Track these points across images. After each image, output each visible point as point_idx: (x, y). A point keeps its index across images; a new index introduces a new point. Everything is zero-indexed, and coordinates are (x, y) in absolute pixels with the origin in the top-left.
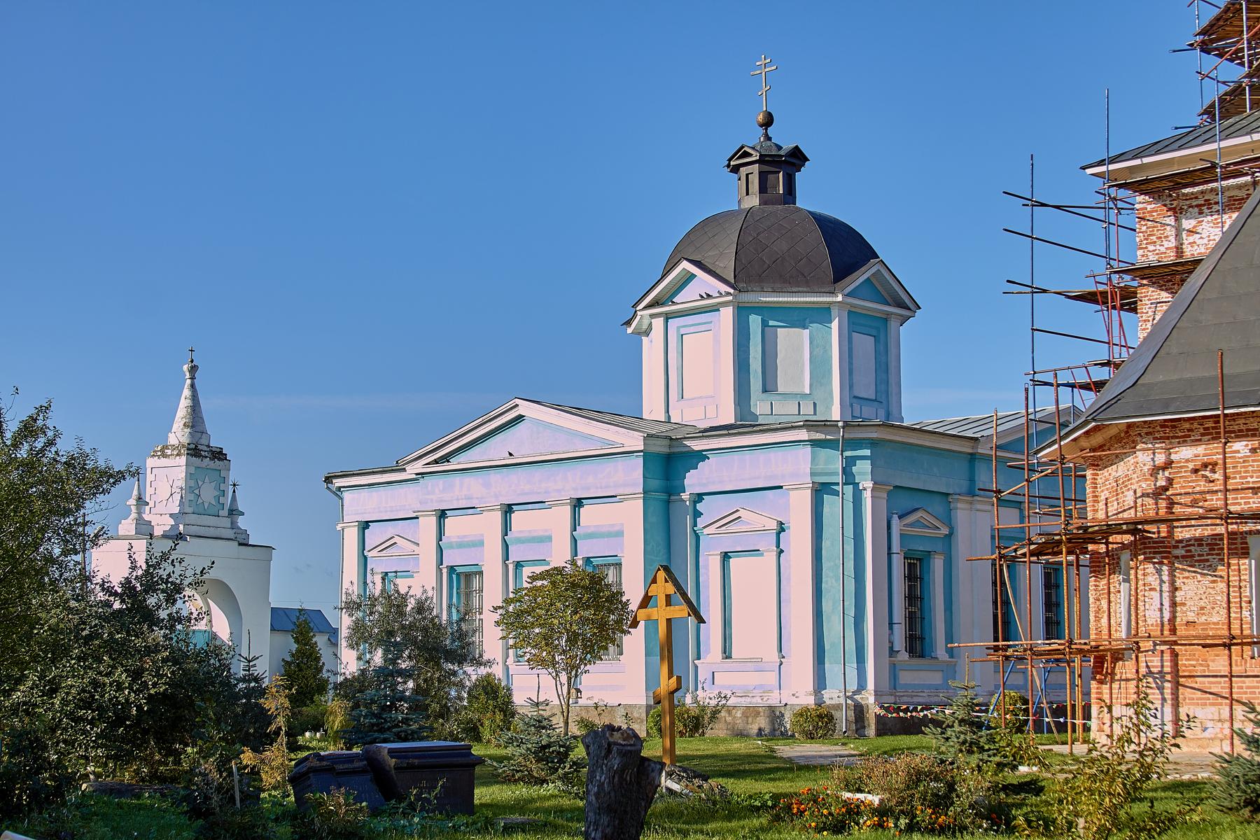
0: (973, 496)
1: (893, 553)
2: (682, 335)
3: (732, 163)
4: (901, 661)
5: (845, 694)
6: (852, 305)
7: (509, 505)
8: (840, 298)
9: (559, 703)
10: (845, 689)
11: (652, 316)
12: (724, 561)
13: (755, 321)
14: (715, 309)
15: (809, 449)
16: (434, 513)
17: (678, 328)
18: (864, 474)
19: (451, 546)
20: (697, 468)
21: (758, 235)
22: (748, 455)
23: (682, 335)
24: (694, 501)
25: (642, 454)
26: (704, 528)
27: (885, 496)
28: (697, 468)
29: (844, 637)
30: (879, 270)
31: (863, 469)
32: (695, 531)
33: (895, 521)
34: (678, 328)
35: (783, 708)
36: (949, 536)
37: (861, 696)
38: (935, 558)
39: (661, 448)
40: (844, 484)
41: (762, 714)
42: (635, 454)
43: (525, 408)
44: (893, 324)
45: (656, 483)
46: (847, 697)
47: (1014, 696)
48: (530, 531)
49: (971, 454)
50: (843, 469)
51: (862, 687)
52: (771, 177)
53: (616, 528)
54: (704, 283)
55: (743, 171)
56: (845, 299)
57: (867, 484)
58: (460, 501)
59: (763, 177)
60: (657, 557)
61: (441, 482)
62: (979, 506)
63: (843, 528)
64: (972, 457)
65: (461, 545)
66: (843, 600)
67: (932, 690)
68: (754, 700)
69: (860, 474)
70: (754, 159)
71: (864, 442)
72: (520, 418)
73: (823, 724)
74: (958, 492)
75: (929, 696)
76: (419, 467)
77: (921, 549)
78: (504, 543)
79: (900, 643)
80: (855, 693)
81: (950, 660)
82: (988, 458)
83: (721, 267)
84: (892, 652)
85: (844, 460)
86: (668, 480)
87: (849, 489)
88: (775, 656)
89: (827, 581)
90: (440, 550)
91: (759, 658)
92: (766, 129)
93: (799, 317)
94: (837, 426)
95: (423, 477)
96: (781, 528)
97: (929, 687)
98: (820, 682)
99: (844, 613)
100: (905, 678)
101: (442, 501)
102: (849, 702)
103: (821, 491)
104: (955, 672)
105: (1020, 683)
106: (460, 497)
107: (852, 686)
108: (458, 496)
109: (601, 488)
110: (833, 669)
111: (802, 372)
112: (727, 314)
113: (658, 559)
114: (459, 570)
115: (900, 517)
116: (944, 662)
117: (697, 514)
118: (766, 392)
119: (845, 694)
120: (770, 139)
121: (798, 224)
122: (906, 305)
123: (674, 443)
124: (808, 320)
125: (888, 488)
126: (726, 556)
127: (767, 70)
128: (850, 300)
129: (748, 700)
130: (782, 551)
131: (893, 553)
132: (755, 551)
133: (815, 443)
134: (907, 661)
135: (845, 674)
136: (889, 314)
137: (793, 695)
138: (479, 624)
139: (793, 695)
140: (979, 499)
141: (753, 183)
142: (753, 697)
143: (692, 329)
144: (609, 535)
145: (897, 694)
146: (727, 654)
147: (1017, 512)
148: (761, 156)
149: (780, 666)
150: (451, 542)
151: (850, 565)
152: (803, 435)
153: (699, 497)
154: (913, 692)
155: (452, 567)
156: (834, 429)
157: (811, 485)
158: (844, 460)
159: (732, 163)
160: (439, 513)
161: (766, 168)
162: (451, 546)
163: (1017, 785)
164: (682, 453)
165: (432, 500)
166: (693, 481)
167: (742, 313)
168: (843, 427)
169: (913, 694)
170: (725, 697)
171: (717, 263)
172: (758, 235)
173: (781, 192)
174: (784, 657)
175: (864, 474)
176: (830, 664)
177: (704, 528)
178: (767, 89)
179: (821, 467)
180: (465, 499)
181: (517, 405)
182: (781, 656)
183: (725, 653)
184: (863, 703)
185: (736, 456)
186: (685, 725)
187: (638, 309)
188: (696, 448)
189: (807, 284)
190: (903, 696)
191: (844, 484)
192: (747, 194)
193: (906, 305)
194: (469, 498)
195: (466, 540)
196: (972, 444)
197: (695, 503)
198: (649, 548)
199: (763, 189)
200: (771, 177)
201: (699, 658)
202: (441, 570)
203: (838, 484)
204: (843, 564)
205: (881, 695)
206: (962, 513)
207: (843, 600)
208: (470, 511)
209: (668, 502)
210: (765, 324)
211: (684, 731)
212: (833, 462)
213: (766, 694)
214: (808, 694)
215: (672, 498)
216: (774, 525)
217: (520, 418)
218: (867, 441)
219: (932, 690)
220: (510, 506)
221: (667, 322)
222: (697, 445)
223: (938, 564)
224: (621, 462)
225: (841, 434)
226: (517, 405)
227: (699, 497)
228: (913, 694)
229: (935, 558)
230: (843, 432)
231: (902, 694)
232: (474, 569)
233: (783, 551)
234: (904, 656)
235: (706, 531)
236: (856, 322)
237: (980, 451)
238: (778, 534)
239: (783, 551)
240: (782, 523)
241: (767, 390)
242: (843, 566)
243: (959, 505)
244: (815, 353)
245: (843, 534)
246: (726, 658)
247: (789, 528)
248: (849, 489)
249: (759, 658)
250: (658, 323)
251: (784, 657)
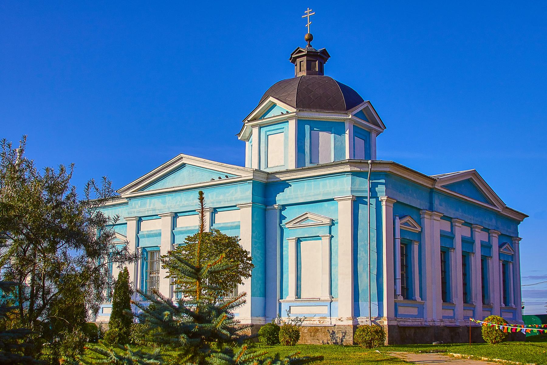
0: (433, 211)
1: (396, 239)
2: (268, 135)
3: (293, 56)
4: (399, 301)
5: (370, 319)
6: (356, 122)
7: (175, 213)
8: (350, 117)
9: (346, 159)
10: (370, 316)
11: (253, 126)
12: (297, 243)
13: (307, 127)
14: (286, 121)
15: (350, 177)
16: (135, 218)
17: (266, 132)
18: (382, 192)
19: (143, 237)
20: (284, 192)
21: (308, 86)
22: (313, 183)
23: (268, 135)
24: (280, 210)
25: (252, 181)
26: (286, 224)
27: (392, 205)
28: (284, 192)
29: (370, 286)
30: (368, 106)
31: (381, 189)
32: (280, 226)
33: (397, 220)
34: (266, 132)
35: (333, 327)
36: (420, 233)
37: (379, 321)
38: (414, 244)
39: (262, 179)
40: (370, 198)
41: (320, 331)
42: (248, 182)
43: (187, 159)
44: (373, 135)
45: (259, 199)
46: (372, 321)
47: (500, 319)
48: (187, 227)
49: (431, 188)
50: (370, 189)
51: (380, 316)
52: (313, 63)
53: (236, 224)
54: (281, 108)
55: (298, 60)
56: (353, 117)
57: (383, 198)
58: (149, 212)
59: (309, 63)
60: (258, 240)
61: (140, 202)
62: (435, 218)
63: (369, 222)
64: (432, 191)
65: (149, 236)
66: (370, 264)
67: (414, 318)
68: (315, 322)
69: (380, 192)
70: (304, 53)
71: (382, 173)
72: (183, 165)
73: (378, 336)
74: (425, 208)
75: (412, 321)
76: (128, 194)
77: (408, 238)
78: (172, 234)
79: (399, 292)
80: (376, 319)
81: (421, 301)
82: (440, 192)
83: (289, 100)
84: (396, 296)
85: (370, 184)
86: (265, 198)
87: (373, 201)
88: (328, 297)
89: (360, 253)
90: (138, 239)
91: (318, 298)
92: (309, 42)
93: (329, 127)
94: (367, 163)
95: (130, 200)
96: (333, 223)
97: (412, 316)
98: (356, 312)
99: (370, 272)
100: (402, 310)
101: (139, 212)
102: (373, 324)
103: (357, 202)
104: (424, 308)
105: (451, 315)
106: (149, 210)
107: (375, 315)
108: (148, 209)
109: (228, 201)
110: (363, 305)
111: (330, 154)
112: (292, 125)
113: (259, 241)
114: (148, 249)
115: (400, 218)
116: (419, 302)
117: (282, 218)
118: (312, 163)
119: (370, 319)
120: (311, 46)
121: (327, 82)
122: (380, 125)
123: (270, 176)
124: (333, 128)
125: (394, 201)
126: (298, 241)
127: (310, 15)
128: (355, 118)
129: (312, 322)
130: (332, 237)
131: (396, 239)
132: (317, 237)
133: (354, 174)
134: (402, 301)
135: (370, 307)
136: (371, 129)
137: (339, 320)
138: (157, 279)
139: (339, 320)
140: (436, 213)
141: (303, 66)
142: (314, 320)
143: (273, 132)
144: (232, 228)
145: (398, 320)
146: (298, 294)
147: (449, 223)
148: (308, 52)
149: (331, 303)
150: (144, 234)
151: (374, 244)
152: (348, 168)
153: (284, 207)
154: (405, 319)
155: (144, 248)
156: (366, 164)
157: (351, 197)
158: (370, 184)
159: (293, 56)
160: (138, 218)
161: (310, 59)
162: (143, 237)
163: (276, 361)
164: (273, 182)
165: (134, 212)
166: (281, 198)
167: (300, 124)
168: (371, 164)
169: (405, 320)
170: (300, 320)
171: (287, 99)
172: (308, 86)
173: (317, 70)
174: (333, 298)
175: (382, 192)
176: (361, 302)
177: (286, 224)
178: (310, 23)
179: (356, 187)
180: (152, 210)
181: (182, 158)
182: (331, 297)
183: (297, 295)
184: (381, 324)
185: (305, 183)
186: (290, 337)
187: (245, 122)
188: (282, 179)
189: (333, 109)
190: (401, 321)
191: (370, 198)
192: (300, 71)
193: (380, 125)
194: (154, 210)
195: (151, 233)
196: (432, 183)
197: (281, 211)
198: (254, 235)
199: (309, 68)
200: (313, 63)
201: (282, 298)
202: (138, 249)
203: (366, 197)
204: (370, 243)
205: (391, 320)
206: (427, 221)
207: (370, 264)
208: (155, 217)
209: (265, 210)
210: (311, 129)
211: (290, 341)
212: (364, 185)
213: (322, 319)
214: (348, 319)
215: (268, 207)
216: (328, 221)
217: (183, 165)
218: (383, 173)
219: (414, 318)
220: (176, 213)
221: (260, 129)
222: (283, 177)
223: (416, 247)
224: (239, 188)
225: (370, 168)
226: (182, 158)
227: (284, 207)
228: (405, 320)
229: (414, 244)
230: (371, 166)
231: (400, 320)
232: (155, 249)
233: (334, 237)
234: (401, 298)
235: (287, 226)
236: (357, 132)
237: (436, 187)
238: (330, 227)
239: (334, 237)
240: (333, 220)
241: (312, 162)
242: (370, 244)
243: (425, 216)
244: (337, 144)
245: (370, 226)
246: (298, 299)
247: (337, 223)
248: (373, 201)
249: (318, 298)
250: (255, 131)
251: (333, 298)
